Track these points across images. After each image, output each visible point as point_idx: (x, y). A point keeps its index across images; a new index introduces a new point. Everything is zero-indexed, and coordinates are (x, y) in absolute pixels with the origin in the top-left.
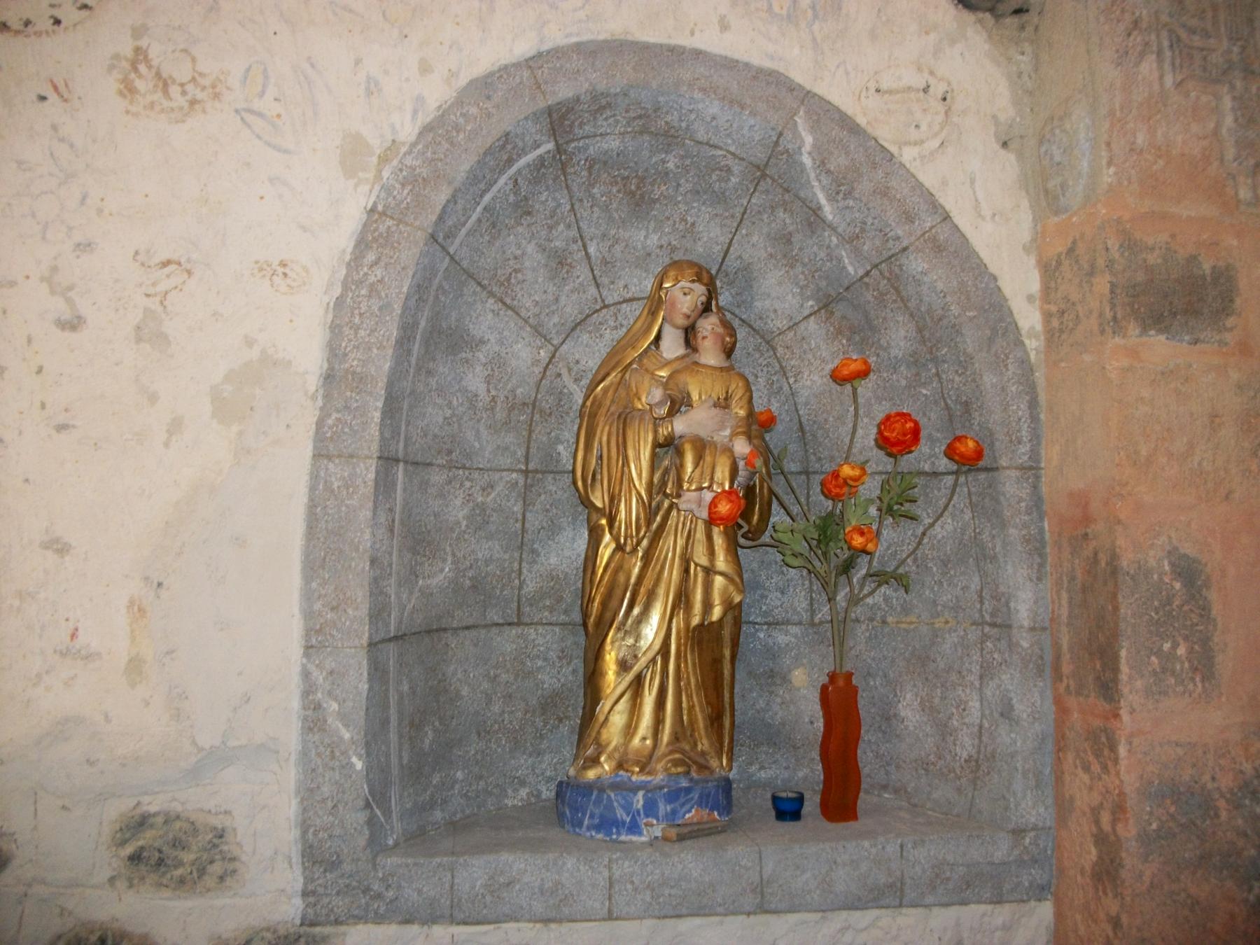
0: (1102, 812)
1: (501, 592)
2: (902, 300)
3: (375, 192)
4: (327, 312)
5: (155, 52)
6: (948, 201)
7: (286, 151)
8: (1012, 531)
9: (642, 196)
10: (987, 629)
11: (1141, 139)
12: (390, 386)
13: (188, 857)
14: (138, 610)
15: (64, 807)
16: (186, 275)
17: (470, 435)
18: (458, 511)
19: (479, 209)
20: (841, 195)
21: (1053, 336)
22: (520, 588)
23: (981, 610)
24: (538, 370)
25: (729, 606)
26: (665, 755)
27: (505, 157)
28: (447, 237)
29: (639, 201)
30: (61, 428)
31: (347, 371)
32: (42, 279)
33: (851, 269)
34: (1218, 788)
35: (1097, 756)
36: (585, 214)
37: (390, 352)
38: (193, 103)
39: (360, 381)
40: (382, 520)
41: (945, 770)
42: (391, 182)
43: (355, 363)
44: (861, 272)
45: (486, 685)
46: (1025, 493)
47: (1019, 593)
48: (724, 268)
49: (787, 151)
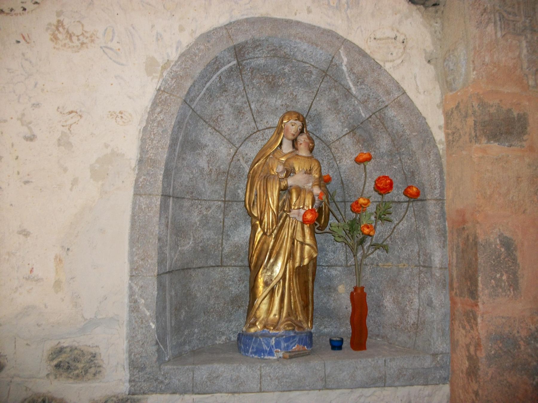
0: (471, 346)
1: (214, 252)
2: (385, 128)
3: (160, 82)
4: (139, 133)
5: (66, 22)
6: (405, 86)
7: (122, 65)
8: (432, 226)
9: (274, 84)
10: (421, 268)
11: (487, 59)
12: (166, 164)
13: (80, 365)
14: (59, 260)
15: (27, 344)
16: (79, 117)
17: (201, 185)
18: (195, 218)
19: (205, 89)
20: (359, 83)
21: (450, 143)
22: (222, 251)
23: (419, 260)
24: (230, 158)
25: (311, 259)
26: (284, 322)
27: (216, 67)
28: (191, 101)
29: (273, 86)
30: (26, 182)
31: (148, 158)
32: (18, 119)
33: (363, 115)
34: (520, 336)
35: (468, 323)
36: (250, 91)
37: (167, 150)
38: (82, 44)
39: (154, 162)
40: (163, 222)
41: (403, 328)
42: (167, 77)
43: (152, 155)
44: (368, 116)
45: (207, 292)
46: (438, 210)
47: (435, 253)
48: (309, 114)
49: (336, 64)
